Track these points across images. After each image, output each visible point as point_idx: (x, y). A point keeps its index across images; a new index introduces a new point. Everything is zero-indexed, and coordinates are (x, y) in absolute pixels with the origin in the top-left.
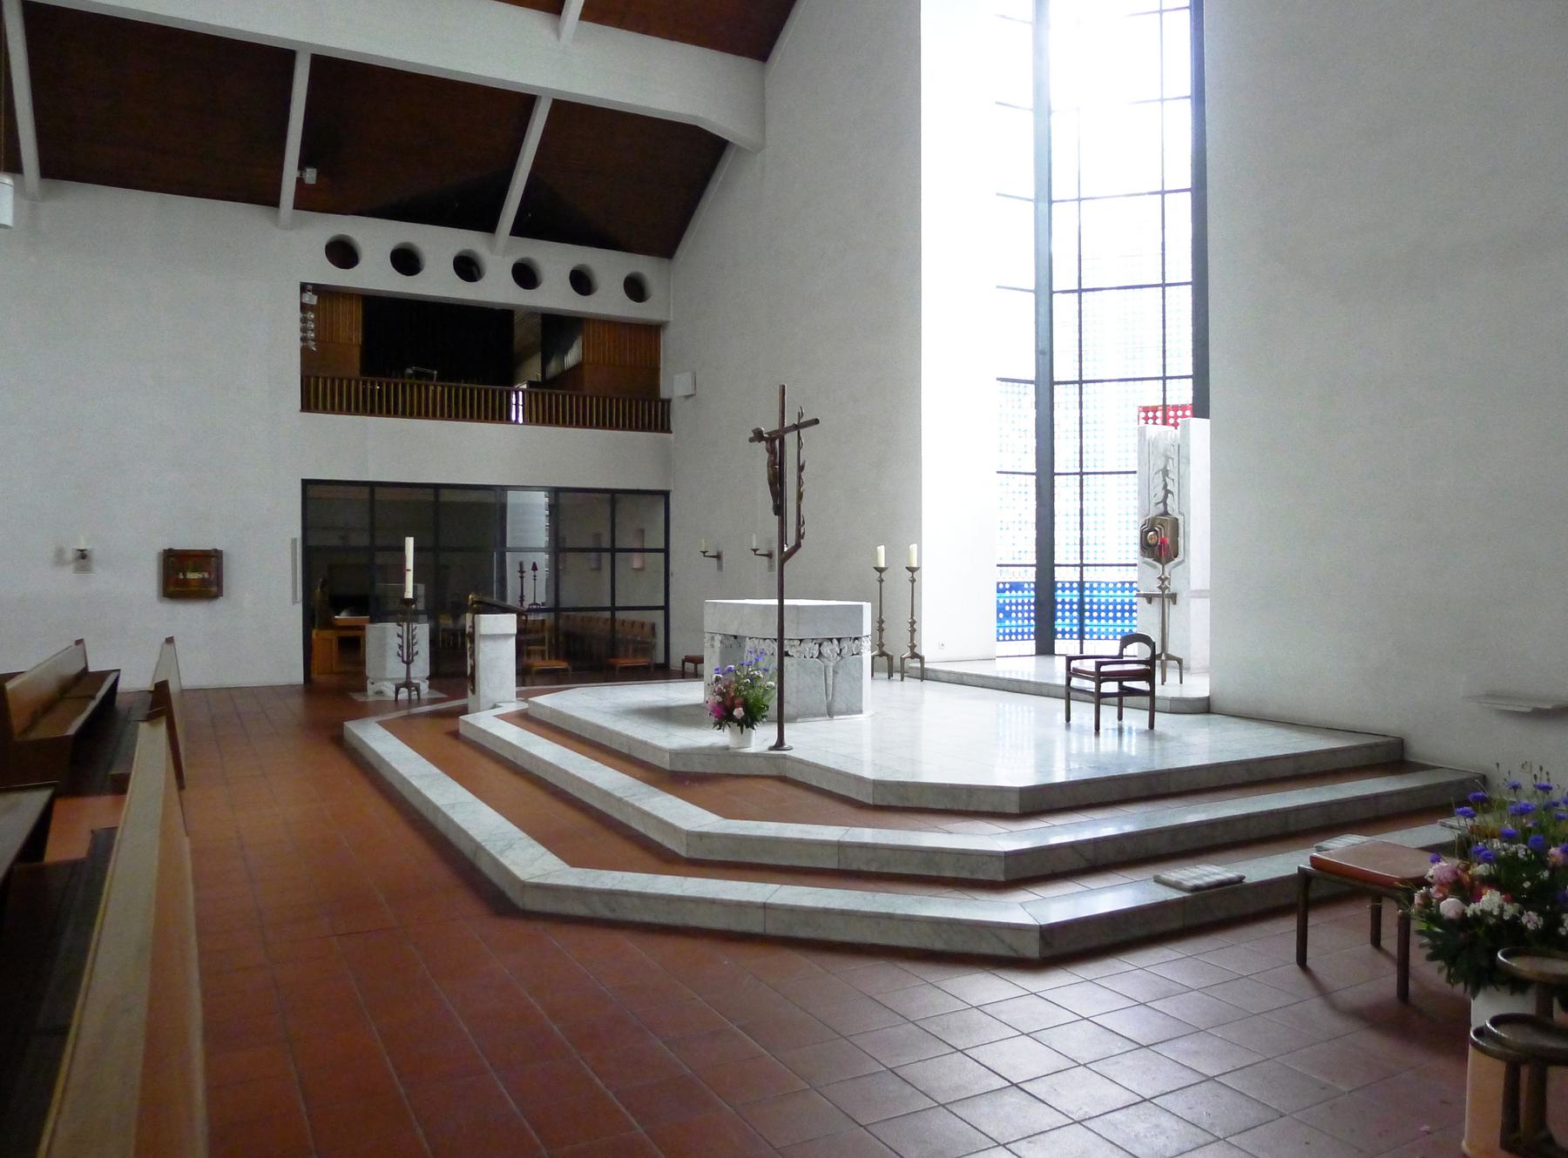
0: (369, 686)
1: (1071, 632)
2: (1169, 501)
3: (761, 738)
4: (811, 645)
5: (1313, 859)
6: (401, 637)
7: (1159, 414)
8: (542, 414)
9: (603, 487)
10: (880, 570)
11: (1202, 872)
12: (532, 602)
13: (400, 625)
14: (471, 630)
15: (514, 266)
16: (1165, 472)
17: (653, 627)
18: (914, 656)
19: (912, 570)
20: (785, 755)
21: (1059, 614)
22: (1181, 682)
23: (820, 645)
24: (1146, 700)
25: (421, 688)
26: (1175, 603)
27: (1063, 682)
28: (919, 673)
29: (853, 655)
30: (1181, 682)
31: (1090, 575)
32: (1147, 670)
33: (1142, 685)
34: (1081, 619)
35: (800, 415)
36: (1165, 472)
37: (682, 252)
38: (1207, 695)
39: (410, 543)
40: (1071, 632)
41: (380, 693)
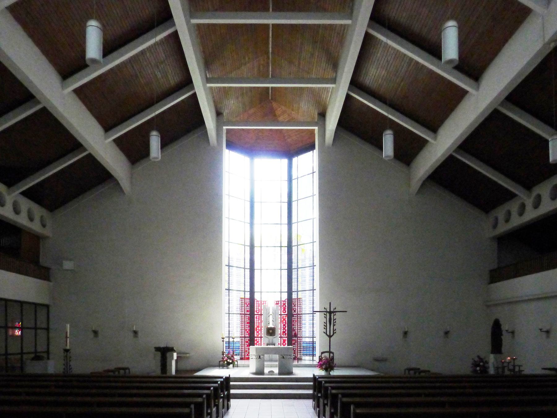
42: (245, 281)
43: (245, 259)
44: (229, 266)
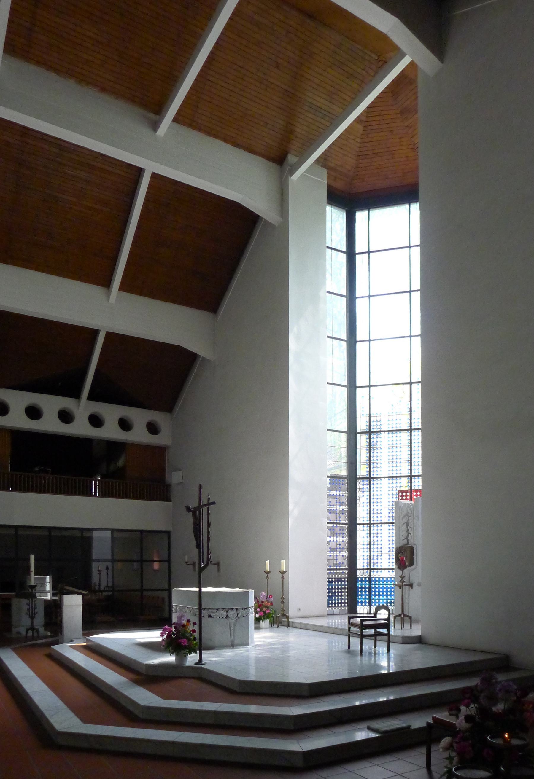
0: (13, 629)
1: (365, 602)
2: (409, 538)
3: (192, 659)
4: (222, 612)
5: (434, 719)
6: (29, 605)
7: (408, 494)
8: (105, 493)
9: (135, 529)
10: (268, 573)
11: (391, 724)
12: (106, 585)
13: (28, 599)
14: (60, 602)
15: (90, 415)
16: (408, 524)
17: (163, 599)
18: (284, 615)
19: (283, 573)
20: (202, 667)
21: (360, 593)
22: (411, 628)
23: (227, 611)
24: (386, 638)
25: (40, 630)
26: (412, 588)
27: (347, 628)
28: (286, 624)
29: (244, 616)
30: (411, 628)
31: (374, 574)
32: (386, 623)
33: (385, 631)
34: (370, 595)
35: (209, 499)
36: (408, 524)
37: (177, 408)
38: (420, 635)
39: (33, 557)
40: (365, 602)
41: (19, 633)
42: (411, 443)
43: (411, 411)
44: (370, 433)
